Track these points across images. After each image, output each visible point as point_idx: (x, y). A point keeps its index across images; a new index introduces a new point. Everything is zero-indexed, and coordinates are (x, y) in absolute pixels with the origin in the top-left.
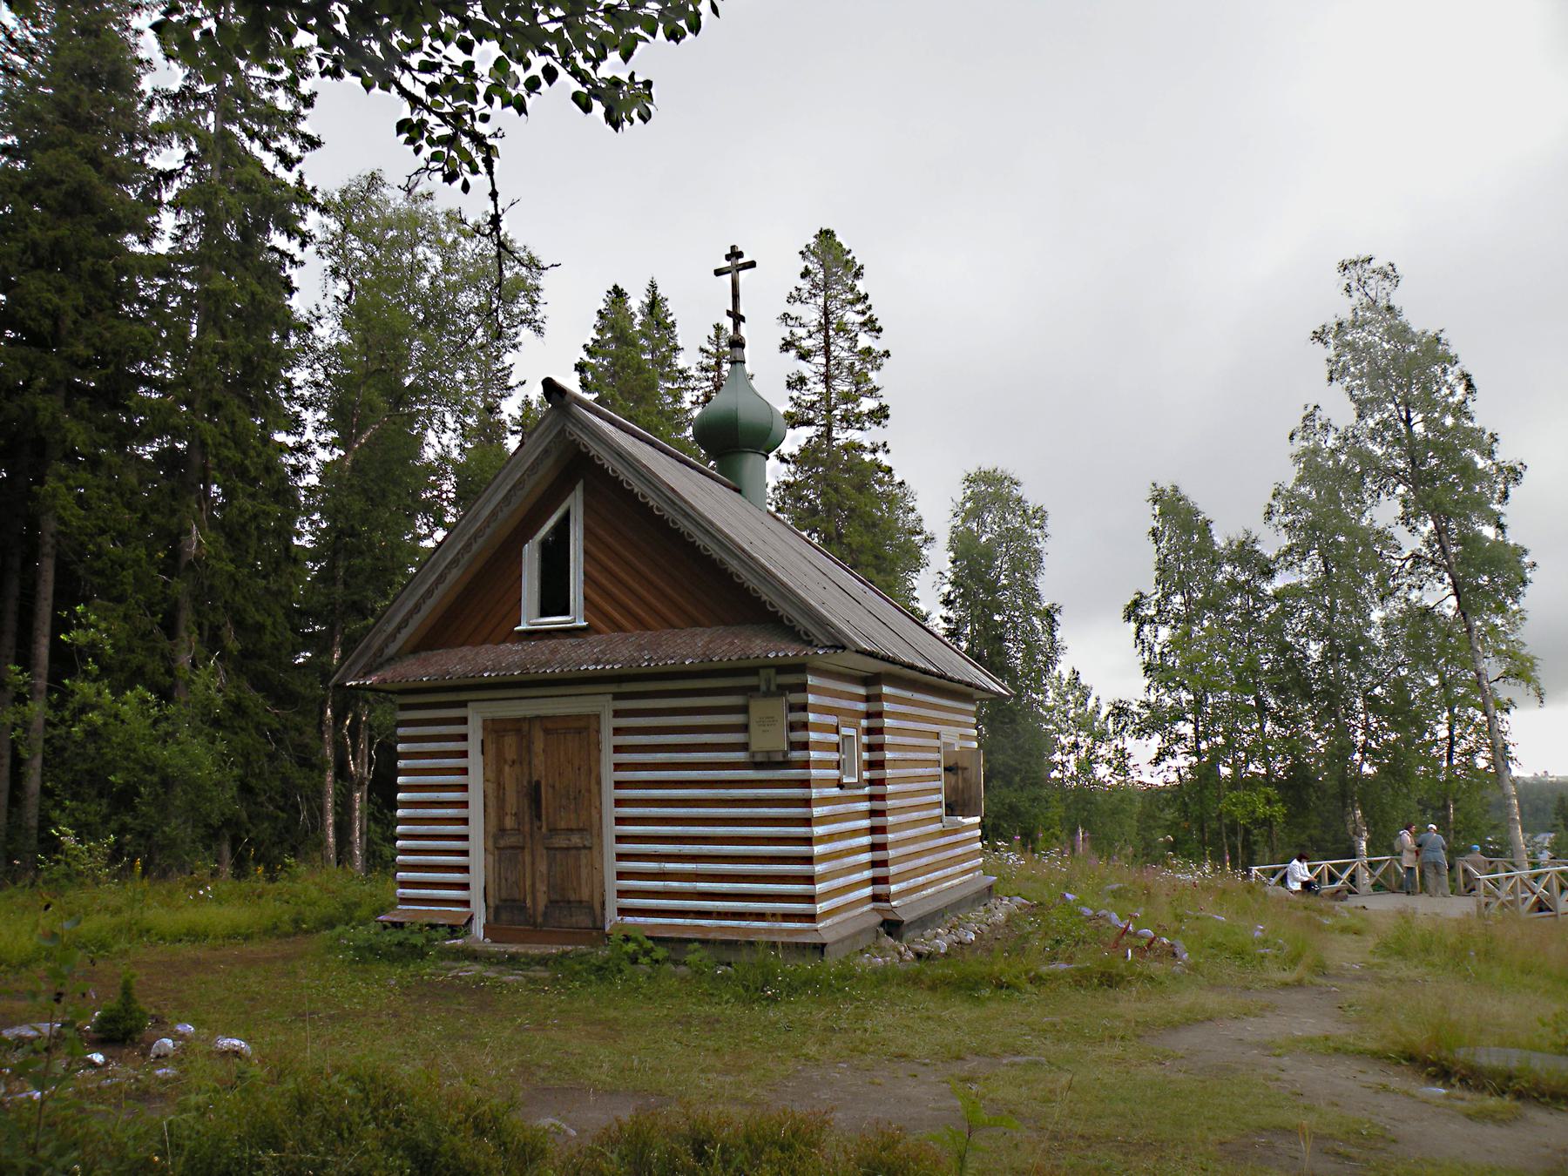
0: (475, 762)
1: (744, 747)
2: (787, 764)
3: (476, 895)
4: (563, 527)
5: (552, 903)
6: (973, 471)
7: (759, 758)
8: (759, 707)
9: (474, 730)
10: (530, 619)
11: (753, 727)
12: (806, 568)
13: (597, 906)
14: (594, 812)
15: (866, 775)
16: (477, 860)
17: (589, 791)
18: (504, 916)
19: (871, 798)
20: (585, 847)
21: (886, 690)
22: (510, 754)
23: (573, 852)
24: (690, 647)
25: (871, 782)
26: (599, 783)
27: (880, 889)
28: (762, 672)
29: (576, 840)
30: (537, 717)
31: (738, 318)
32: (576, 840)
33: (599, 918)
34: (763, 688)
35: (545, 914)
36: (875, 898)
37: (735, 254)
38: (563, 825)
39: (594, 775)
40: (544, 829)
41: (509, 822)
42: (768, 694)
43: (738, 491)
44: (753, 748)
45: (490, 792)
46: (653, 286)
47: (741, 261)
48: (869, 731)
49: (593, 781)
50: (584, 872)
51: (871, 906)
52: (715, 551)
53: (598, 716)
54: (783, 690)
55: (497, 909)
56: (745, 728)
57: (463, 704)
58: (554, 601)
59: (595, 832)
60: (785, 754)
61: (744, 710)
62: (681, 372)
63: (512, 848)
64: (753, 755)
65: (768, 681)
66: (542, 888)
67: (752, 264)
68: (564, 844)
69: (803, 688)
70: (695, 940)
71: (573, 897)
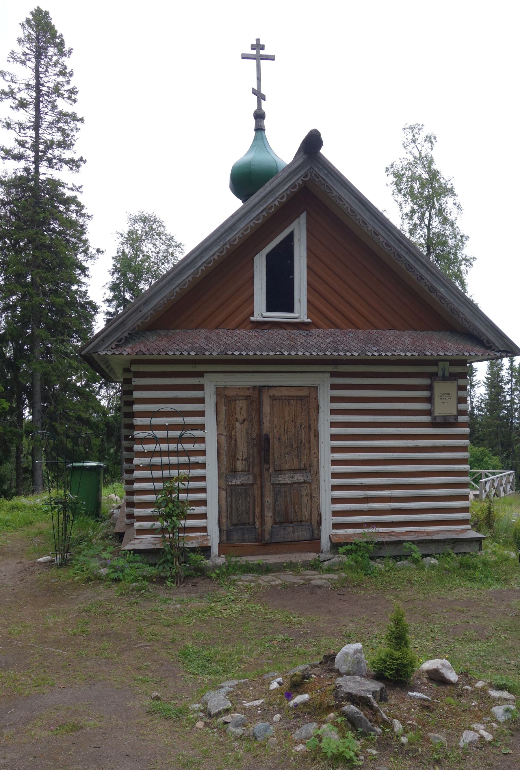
1: (428, 412)
4: (287, 248)
6: (136, 213)
7: (438, 420)
8: (440, 388)
10: (260, 311)
13: (314, 523)
18: (236, 536)
24: (402, 344)
26: (317, 436)
28: (440, 363)
30: (266, 386)
31: (260, 96)
33: (316, 532)
34: (440, 374)
35: (271, 533)
37: (258, 46)
38: (287, 467)
39: (313, 430)
42: (444, 378)
44: (436, 413)
47: (262, 52)
50: (305, 500)
56: (429, 400)
57: (201, 375)
58: (280, 296)
60: (456, 418)
61: (429, 388)
64: (435, 418)
65: (444, 370)
67: (271, 58)
70: (408, 541)
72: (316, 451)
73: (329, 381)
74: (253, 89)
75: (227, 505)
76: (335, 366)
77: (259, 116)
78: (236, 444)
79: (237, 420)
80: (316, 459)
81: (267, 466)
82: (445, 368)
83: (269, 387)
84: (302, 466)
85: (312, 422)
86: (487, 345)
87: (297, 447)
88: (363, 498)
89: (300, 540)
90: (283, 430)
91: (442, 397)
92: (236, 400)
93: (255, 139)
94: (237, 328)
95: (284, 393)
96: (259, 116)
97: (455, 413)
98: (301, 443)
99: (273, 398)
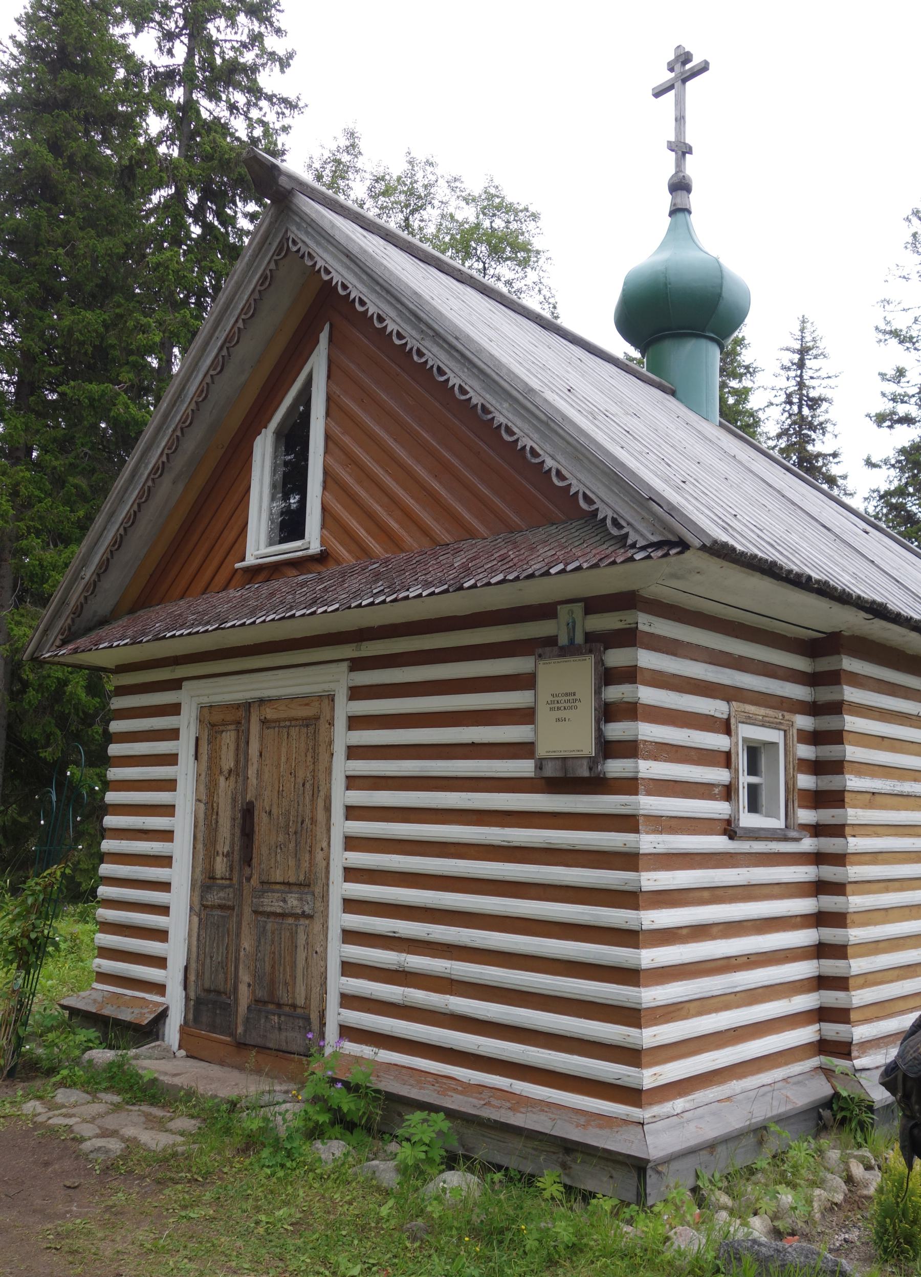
0: (185, 772)
1: (523, 750)
2: (598, 784)
3: (172, 977)
5: (257, 1003)
9: (187, 724)
10: (259, 547)
11: (543, 714)
12: (723, 467)
13: (314, 1017)
14: (320, 856)
15: (806, 816)
16: (179, 923)
17: (313, 821)
19: (818, 858)
20: (304, 915)
21: (850, 664)
22: (228, 761)
23: (290, 921)
25: (817, 830)
26: (328, 809)
27: (833, 1030)
28: (562, 610)
29: (293, 901)
32: (293, 901)
34: (563, 640)
35: (247, 1020)
36: (823, 1046)
37: (684, 57)
40: (254, 881)
41: (220, 866)
42: (569, 651)
43: (673, 393)
44: (541, 752)
45: (201, 816)
46: (782, 349)
48: (815, 738)
49: (320, 804)
50: (301, 955)
51: (815, 1061)
52: (478, 395)
53: (331, 698)
54: (600, 642)
55: (199, 1002)
56: (526, 716)
57: (176, 685)
58: (290, 525)
59: (318, 890)
62: (747, 367)
63: (221, 907)
66: (245, 977)
68: (277, 907)
69: (629, 638)
71: (285, 1000)
72: (324, 845)
73: (338, 680)
74: (669, 142)
75: (198, 947)
76: (362, 644)
77: (680, 186)
78: (217, 822)
79: (221, 772)
80: (324, 863)
81: (247, 871)
82: (574, 622)
83: (262, 701)
84: (302, 878)
85: (322, 776)
86: (615, 532)
87: (296, 833)
88: (397, 971)
89: (289, 1049)
90: (276, 793)
91: (555, 704)
92: (223, 731)
93: (672, 229)
94: (225, 588)
95: (281, 712)
96: (680, 186)
97: (589, 748)
98: (302, 822)
99: (264, 722)
